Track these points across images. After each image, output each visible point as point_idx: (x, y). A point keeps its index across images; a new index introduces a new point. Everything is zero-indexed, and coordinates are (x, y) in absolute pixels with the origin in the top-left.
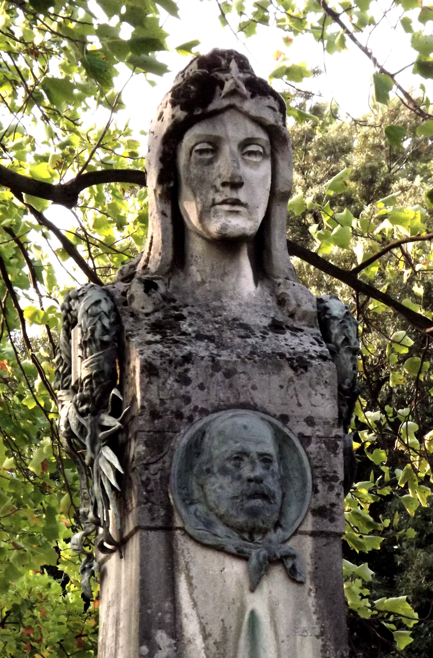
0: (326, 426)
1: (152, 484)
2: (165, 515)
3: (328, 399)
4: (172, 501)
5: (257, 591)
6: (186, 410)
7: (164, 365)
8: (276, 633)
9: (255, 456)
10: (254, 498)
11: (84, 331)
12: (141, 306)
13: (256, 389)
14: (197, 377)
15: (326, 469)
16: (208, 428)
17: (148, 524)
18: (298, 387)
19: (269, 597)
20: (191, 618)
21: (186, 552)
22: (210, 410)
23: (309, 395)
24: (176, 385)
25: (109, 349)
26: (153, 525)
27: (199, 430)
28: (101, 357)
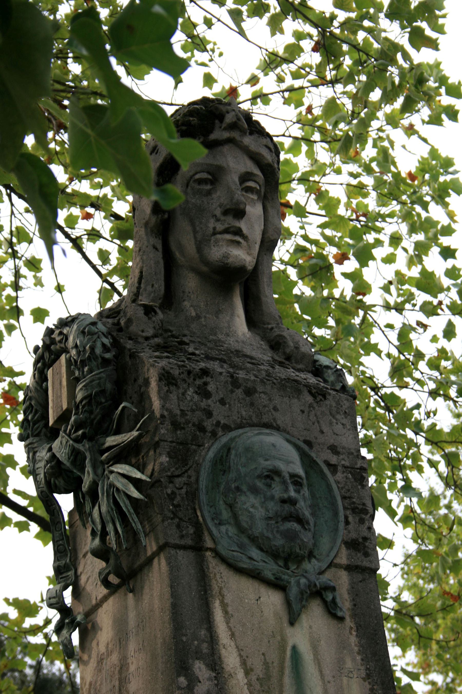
0: (350, 456)
1: (178, 498)
2: (195, 533)
3: (349, 430)
4: (200, 518)
5: (297, 625)
6: (209, 424)
7: (182, 376)
8: (321, 672)
9: (287, 477)
10: (290, 521)
11: (81, 349)
12: (141, 329)
13: (278, 410)
14: (217, 392)
15: (354, 500)
16: (233, 444)
17: (177, 542)
18: (318, 413)
19: (310, 633)
20: (229, 649)
21: (218, 576)
22: (233, 426)
23: (331, 423)
24: (196, 396)
25: (110, 368)
26: (183, 542)
27: (225, 446)
28: (103, 375)
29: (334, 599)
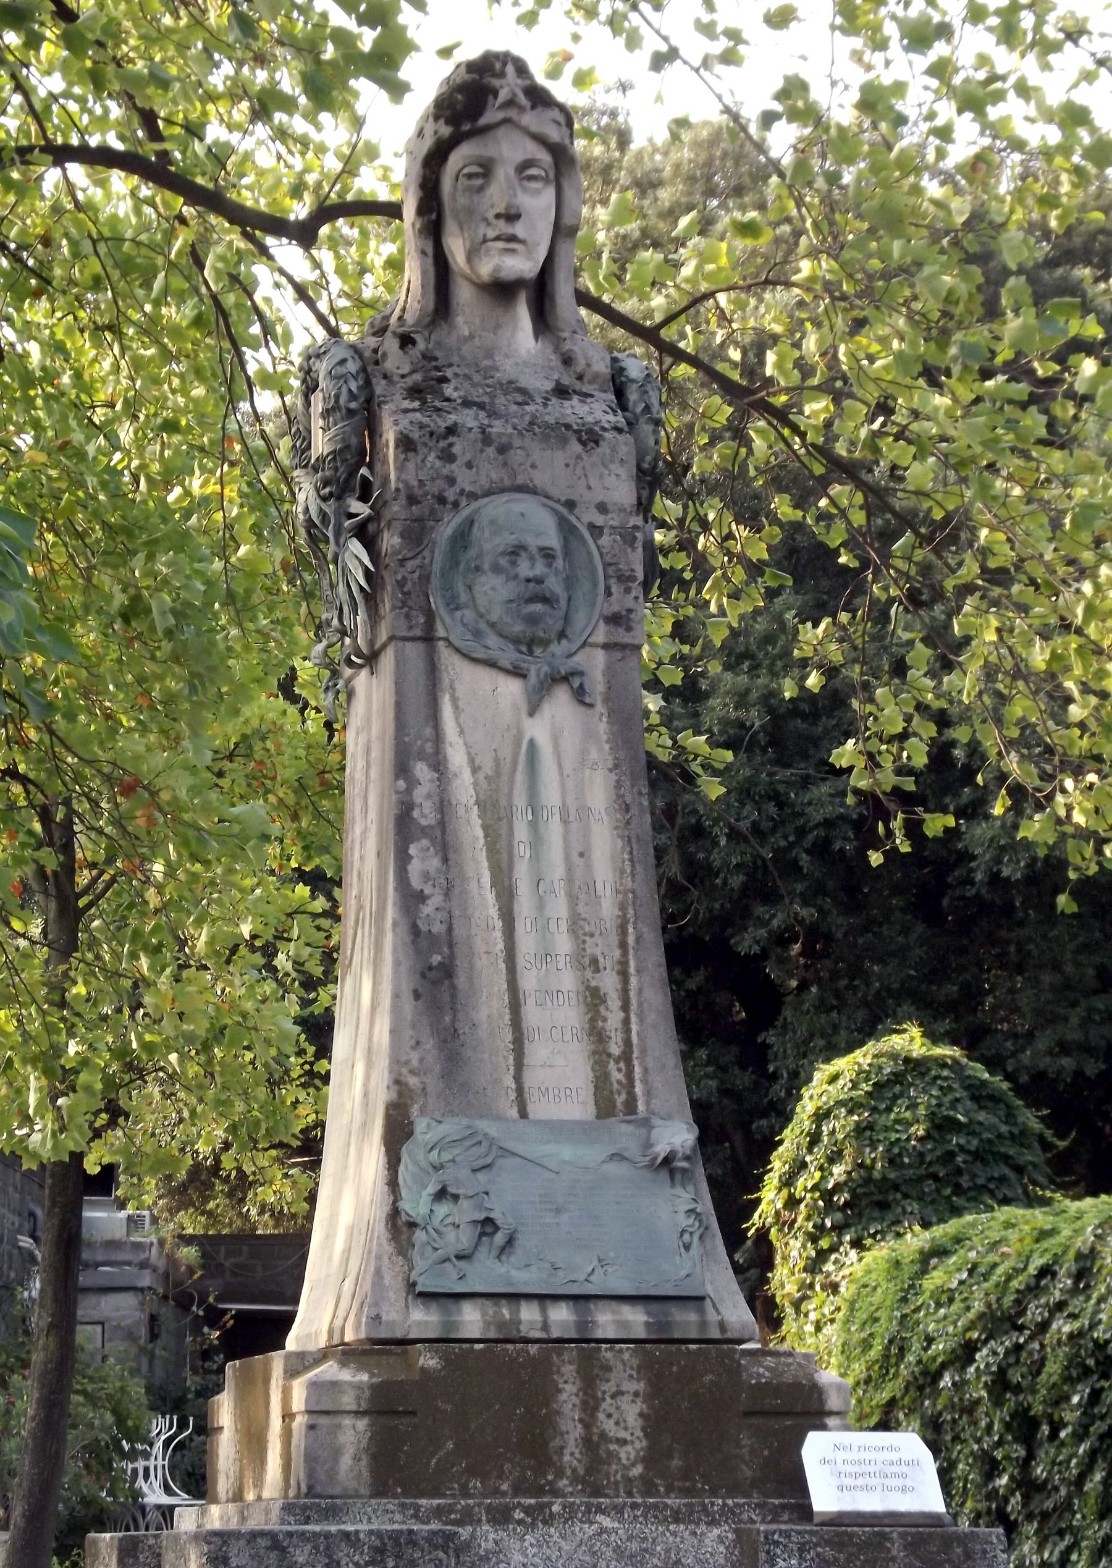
6: (451, 494)
9: (534, 551)
23: (601, 476)
29: (581, 686)
